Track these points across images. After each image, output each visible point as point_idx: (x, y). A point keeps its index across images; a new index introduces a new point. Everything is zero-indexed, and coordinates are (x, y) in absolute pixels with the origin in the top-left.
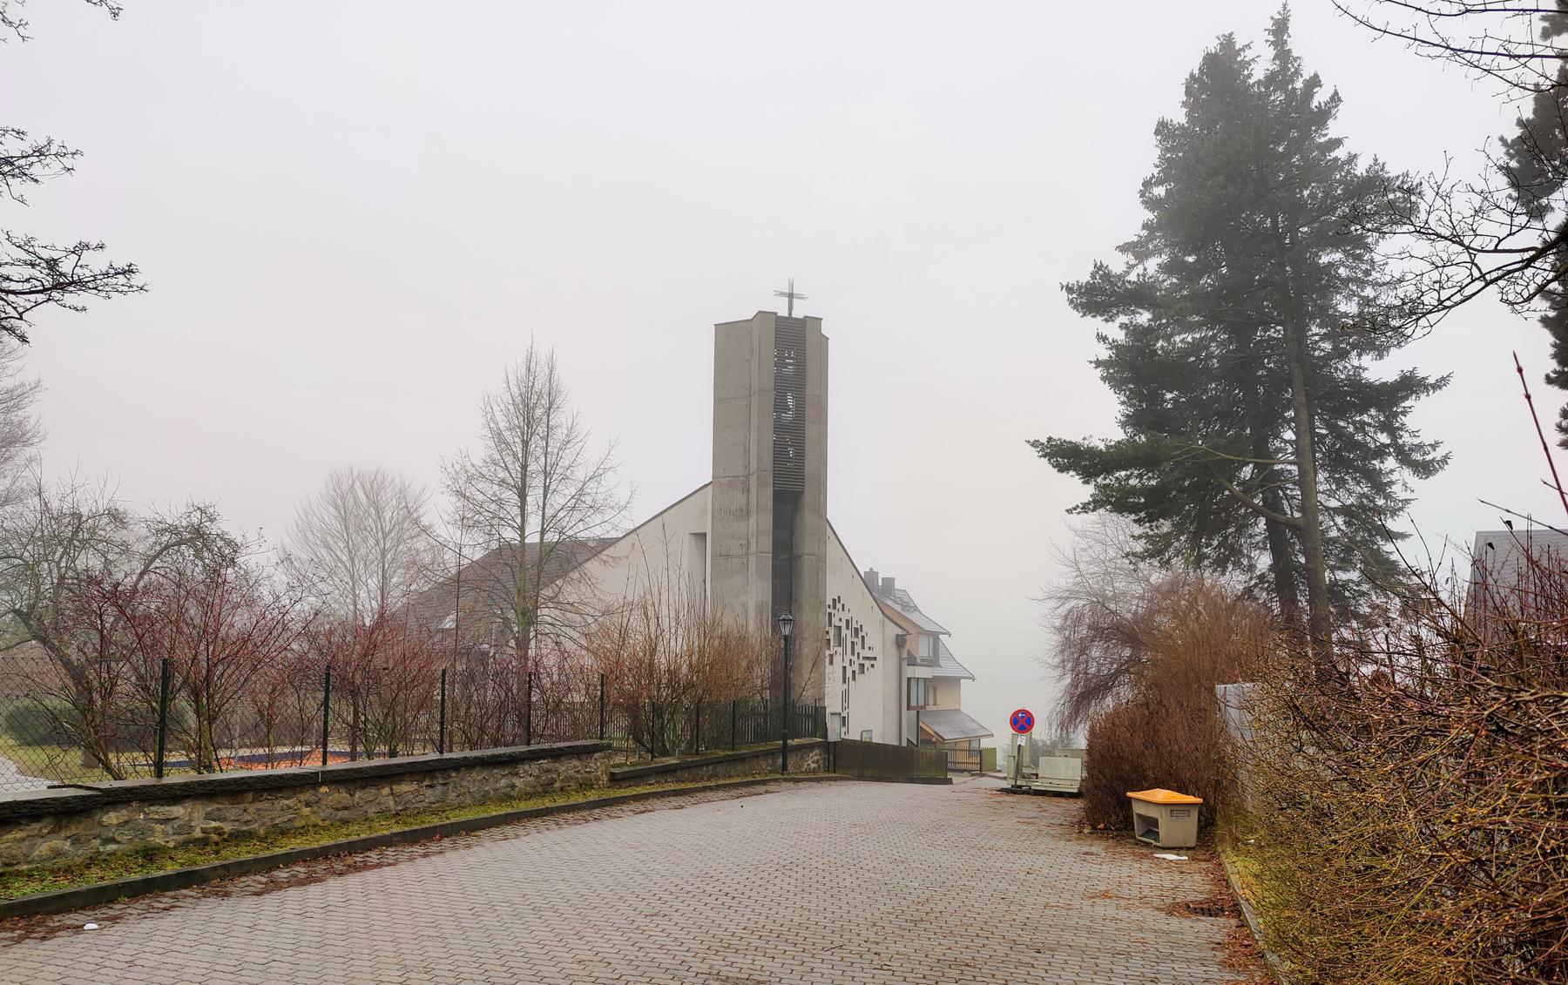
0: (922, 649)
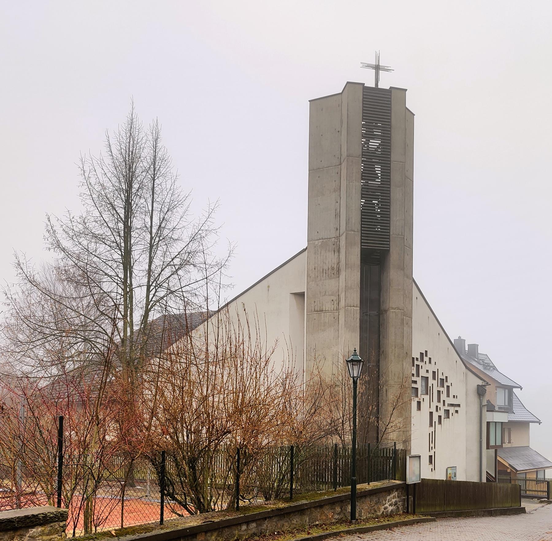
0: (500, 400)
